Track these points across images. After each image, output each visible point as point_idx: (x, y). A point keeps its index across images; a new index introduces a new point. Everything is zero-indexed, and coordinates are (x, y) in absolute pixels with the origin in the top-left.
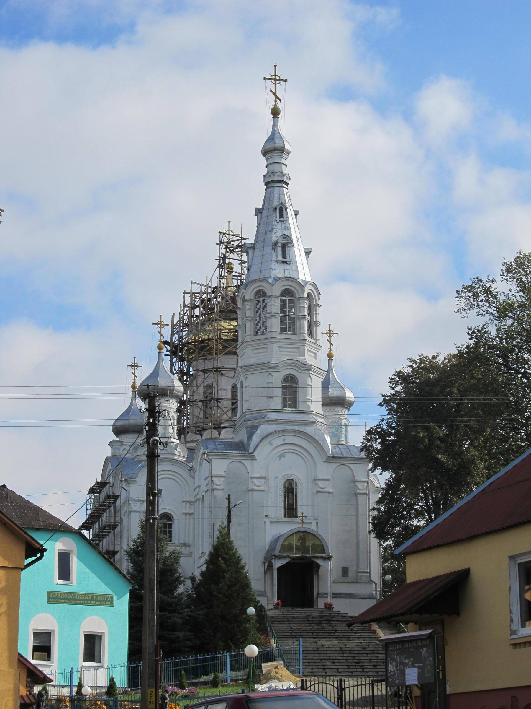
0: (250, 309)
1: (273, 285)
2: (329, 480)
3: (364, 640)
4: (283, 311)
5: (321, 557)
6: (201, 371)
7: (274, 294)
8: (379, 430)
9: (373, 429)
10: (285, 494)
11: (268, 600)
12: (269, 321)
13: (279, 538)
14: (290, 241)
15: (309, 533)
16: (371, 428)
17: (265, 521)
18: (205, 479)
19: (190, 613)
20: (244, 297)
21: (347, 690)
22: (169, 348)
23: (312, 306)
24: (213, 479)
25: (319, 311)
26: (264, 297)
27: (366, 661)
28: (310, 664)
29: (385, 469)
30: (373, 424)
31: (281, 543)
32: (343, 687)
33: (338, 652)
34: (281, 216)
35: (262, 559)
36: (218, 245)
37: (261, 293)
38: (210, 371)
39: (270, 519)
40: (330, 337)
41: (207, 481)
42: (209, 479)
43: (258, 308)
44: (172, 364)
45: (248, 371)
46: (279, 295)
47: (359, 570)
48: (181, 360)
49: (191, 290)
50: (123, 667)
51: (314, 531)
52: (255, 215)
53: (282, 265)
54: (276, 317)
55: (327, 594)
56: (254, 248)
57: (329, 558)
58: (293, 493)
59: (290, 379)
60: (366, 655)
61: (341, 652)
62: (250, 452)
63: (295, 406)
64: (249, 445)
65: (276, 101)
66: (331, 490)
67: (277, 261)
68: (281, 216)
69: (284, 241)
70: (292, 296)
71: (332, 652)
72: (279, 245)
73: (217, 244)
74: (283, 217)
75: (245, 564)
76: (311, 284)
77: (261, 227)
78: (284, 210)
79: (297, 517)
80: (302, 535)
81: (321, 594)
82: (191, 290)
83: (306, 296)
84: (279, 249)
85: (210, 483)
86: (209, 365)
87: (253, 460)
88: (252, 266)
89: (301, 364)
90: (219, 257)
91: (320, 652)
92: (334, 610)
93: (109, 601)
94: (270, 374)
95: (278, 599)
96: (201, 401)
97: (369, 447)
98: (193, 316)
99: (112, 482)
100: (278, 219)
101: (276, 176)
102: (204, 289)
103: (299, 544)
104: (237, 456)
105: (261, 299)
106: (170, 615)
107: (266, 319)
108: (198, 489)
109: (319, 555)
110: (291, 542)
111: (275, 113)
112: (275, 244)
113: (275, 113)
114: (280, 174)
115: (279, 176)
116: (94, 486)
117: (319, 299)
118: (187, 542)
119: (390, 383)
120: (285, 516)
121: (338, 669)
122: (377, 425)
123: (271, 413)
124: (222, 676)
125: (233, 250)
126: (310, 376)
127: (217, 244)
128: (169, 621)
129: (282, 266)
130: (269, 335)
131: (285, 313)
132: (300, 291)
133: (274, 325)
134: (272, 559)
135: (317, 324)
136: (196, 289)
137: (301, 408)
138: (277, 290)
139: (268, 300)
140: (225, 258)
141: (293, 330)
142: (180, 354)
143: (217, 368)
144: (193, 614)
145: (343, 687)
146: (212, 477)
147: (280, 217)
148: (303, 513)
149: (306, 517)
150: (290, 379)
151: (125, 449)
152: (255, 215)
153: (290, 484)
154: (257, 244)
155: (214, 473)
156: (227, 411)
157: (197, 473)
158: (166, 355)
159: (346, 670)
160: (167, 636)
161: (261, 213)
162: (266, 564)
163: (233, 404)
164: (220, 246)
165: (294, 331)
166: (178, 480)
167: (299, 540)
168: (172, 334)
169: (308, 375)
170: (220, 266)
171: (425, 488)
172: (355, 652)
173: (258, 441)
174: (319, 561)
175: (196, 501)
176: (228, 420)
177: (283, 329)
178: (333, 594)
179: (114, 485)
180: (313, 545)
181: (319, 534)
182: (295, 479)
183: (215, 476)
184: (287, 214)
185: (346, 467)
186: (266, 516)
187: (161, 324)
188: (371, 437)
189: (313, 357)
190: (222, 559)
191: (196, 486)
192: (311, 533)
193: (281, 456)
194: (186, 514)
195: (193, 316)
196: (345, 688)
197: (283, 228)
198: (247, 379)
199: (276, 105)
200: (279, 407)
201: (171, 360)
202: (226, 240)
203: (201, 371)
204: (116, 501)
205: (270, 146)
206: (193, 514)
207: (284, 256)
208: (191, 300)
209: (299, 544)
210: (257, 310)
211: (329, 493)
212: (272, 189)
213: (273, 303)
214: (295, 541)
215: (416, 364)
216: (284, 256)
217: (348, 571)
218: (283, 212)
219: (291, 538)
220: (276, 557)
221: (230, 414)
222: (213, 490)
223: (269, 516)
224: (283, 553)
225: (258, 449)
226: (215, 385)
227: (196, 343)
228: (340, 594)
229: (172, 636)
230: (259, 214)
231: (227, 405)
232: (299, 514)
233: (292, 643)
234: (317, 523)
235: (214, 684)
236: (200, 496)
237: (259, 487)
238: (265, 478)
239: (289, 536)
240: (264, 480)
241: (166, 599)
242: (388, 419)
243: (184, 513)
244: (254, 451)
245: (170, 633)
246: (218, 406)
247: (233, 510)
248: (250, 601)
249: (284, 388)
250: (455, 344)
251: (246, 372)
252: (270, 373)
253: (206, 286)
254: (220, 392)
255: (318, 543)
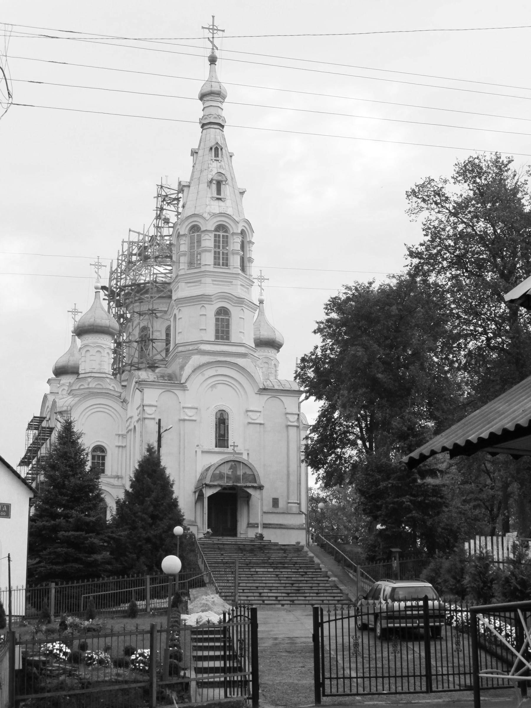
0: (185, 244)
1: (207, 220)
2: (260, 412)
3: (300, 567)
4: (217, 246)
5: (253, 487)
6: (137, 313)
7: (208, 229)
8: (313, 357)
9: (307, 356)
10: (216, 425)
11: (198, 530)
12: (203, 255)
13: (209, 467)
14: (225, 179)
15: (240, 462)
16: (305, 355)
17: (196, 452)
18: (137, 409)
19: (111, 535)
20: (179, 233)
21: (326, 626)
22: (107, 293)
23: (245, 243)
24: (145, 408)
25: (254, 248)
26: (198, 232)
27: (306, 588)
28: (245, 591)
29: (319, 398)
30: (307, 350)
31: (212, 472)
32: (320, 621)
33: (274, 579)
34: (217, 155)
35: (193, 489)
36: (156, 199)
37: (195, 228)
38: (145, 314)
39: (201, 450)
40: (213, 34)
41: (139, 410)
42: (141, 408)
43: (192, 243)
44: (109, 307)
45: (182, 304)
46: (213, 229)
47: (290, 501)
48: (119, 305)
49: (129, 239)
50: (21, 591)
51: (244, 460)
52: (191, 155)
53: (217, 201)
54: (210, 251)
55: (258, 524)
56: (189, 186)
57: (261, 488)
58: (224, 423)
59: (223, 312)
60: (305, 582)
61: (277, 579)
62: (182, 382)
63: (228, 338)
64: (181, 375)
65: (213, 49)
66: (262, 422)
67: (212, 198)
68: (217, 155)
69: (220, 178)
70: (226, 231)
71: (267, 579)
72: (214, 182)
73: (154, 197)
74: (218, 157)
75: (173, 481)
76: (245, 221)
77: (196, 166)
78: (220, 150)
79: (228, 447)
80: (233, 464)
81: (251, 524)
82: (129, 239)
83: (239, 232)
84: (214, 187)
85: (141, 412)
86: (144, 308)
87: (185, 390)
88: (188, 203)
89: (234, 297)
90: (157, 208)
91: (255, 578)
92: (264, 539)
93: (5, 511)
94: (203, 306)
95: (208, 528)
96: (136, 342)
97: (302, 375)
98: (130, 262)
99: (48, 417)
100: (213, 158)
101: (212, 118)
102: (141, 237)
103: (230, 473)
104: (167, 386)
105: (196, 234)
106: (87, 535)
107: (200, 254)
108: (130, 420)
109: (250, 485)
110: (222, 471)
111: (213, 60)
112: (211, 182)
113: (213, 60)
114: (216, 116)
115: (215, 118)
116: (32, 421)
117: (252, 236)
118: (119, 474)
119: (326, 308)
120: (216, 447)
121: (277, 597)
122: (311, 352)
123: (203, 345)
124: (141, 604)
125: (170, 203)
126: (242, 309)
127: (154, 197)
128: (86, 542)
129: (217, 203)
130: (203, 269)
131: (219, 248)
132: (234, 226)
133: (208, 259)
134: (203, 487)
135: (250, 260)
136: (134, 238)
137: (234, 338)
138: (211, 225)
139: (202, 235)
140: (162, 209)
141: (226, 264)
142: (118, 298)
143: (152, 310)
144: (114, 535)
145: (320, 621)
146: (143, 406)
147: (215, 156)
148: (234, 443)
149: (237, 446)
150: (223, 312)
151: (64, 389)
152: (191, 155)
153: (222, 414)
154: (192, 182)
155: (145, 403)
156: (161, 351)
157: (129, 405)
158: (104, 299)
159: (285, 598)
160: (84, 558)
161: (197, 153)
162: (197, 494)
163: (167, 345)
164: (158, 199)
165: (227, 265)
166: (111, 413)
167: (230, 469)
168: (111, 280)
169: (241, 308)
170: (158, 217)
171: (362, 412)
172: (293, 579)
173: (190, 371)
174: (250, 491)
175: (128, 432)
176: (162, 360)
177: (216, 264)
178: (264, 524)
179: (50, 419)
180: (245, 474)
181: (251, 464)
182: (227, 410)
183: (147, 406)
184: (222, 154)
185: (277, 399)
186: (198, 446)
187: (98, 265)
188: (304, 365)
189: (246, 292)
190: (148, 476)
191: (128, 417)
192: (243, 463)
193: (213, 386)
194: (119, 447)
195: (130, 262)
196: (322, 622)
197: (218, 166)
198: (180, 312)
199: (213, 53)
200: (212, 338)
201: (109, 304)
202: (164, 194)
203: (137, 313)
204: (51, 434)
205: (207, 89)
206: (125, 446)
207: (219, 192)
208: (129, 248)
209: (230, 473)
210: (192, 247)
211: (261, 424)
212: (208, 130)
213: (207, 237)
214: (226, 470)
215: (351, 291)
216: (219, 192)
217: (278, 501)
218: (218, 152)
219: (222, 467)
220: (207, 485)
221: (164, 354)
222: (145, 419)
223: (200, 446)
224: (214, 481)
225: (190, 379)
226: (150, 326)
227: (133, 287)
228: (270, 524)
229: (89, 559)
230: (195, 155)
231: (160, 346)
232: (230, 443)
233: (223, 570)
234: (248, 454)
235: (133, 613)
236: (132, 427)
237: (190, 417)
238: (197, 408)
239: (220, 465)
240: (195, 411)
241: (83, 517)
242: (322, 347)
243: (117, 446)
244: (186, 381)
245: (87, 555)
246: (153, 347)
247: (165, 436)
248: (179, 521)
249: (217, 320)
250: (405, 245)
251: (179, 304)
252: (205, 305)
253: (143, 234)
254: (155, 333)
255: (249, 472)
